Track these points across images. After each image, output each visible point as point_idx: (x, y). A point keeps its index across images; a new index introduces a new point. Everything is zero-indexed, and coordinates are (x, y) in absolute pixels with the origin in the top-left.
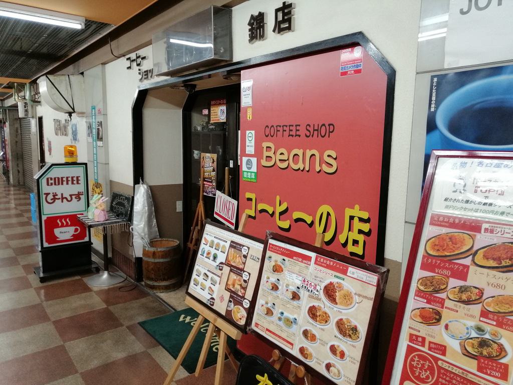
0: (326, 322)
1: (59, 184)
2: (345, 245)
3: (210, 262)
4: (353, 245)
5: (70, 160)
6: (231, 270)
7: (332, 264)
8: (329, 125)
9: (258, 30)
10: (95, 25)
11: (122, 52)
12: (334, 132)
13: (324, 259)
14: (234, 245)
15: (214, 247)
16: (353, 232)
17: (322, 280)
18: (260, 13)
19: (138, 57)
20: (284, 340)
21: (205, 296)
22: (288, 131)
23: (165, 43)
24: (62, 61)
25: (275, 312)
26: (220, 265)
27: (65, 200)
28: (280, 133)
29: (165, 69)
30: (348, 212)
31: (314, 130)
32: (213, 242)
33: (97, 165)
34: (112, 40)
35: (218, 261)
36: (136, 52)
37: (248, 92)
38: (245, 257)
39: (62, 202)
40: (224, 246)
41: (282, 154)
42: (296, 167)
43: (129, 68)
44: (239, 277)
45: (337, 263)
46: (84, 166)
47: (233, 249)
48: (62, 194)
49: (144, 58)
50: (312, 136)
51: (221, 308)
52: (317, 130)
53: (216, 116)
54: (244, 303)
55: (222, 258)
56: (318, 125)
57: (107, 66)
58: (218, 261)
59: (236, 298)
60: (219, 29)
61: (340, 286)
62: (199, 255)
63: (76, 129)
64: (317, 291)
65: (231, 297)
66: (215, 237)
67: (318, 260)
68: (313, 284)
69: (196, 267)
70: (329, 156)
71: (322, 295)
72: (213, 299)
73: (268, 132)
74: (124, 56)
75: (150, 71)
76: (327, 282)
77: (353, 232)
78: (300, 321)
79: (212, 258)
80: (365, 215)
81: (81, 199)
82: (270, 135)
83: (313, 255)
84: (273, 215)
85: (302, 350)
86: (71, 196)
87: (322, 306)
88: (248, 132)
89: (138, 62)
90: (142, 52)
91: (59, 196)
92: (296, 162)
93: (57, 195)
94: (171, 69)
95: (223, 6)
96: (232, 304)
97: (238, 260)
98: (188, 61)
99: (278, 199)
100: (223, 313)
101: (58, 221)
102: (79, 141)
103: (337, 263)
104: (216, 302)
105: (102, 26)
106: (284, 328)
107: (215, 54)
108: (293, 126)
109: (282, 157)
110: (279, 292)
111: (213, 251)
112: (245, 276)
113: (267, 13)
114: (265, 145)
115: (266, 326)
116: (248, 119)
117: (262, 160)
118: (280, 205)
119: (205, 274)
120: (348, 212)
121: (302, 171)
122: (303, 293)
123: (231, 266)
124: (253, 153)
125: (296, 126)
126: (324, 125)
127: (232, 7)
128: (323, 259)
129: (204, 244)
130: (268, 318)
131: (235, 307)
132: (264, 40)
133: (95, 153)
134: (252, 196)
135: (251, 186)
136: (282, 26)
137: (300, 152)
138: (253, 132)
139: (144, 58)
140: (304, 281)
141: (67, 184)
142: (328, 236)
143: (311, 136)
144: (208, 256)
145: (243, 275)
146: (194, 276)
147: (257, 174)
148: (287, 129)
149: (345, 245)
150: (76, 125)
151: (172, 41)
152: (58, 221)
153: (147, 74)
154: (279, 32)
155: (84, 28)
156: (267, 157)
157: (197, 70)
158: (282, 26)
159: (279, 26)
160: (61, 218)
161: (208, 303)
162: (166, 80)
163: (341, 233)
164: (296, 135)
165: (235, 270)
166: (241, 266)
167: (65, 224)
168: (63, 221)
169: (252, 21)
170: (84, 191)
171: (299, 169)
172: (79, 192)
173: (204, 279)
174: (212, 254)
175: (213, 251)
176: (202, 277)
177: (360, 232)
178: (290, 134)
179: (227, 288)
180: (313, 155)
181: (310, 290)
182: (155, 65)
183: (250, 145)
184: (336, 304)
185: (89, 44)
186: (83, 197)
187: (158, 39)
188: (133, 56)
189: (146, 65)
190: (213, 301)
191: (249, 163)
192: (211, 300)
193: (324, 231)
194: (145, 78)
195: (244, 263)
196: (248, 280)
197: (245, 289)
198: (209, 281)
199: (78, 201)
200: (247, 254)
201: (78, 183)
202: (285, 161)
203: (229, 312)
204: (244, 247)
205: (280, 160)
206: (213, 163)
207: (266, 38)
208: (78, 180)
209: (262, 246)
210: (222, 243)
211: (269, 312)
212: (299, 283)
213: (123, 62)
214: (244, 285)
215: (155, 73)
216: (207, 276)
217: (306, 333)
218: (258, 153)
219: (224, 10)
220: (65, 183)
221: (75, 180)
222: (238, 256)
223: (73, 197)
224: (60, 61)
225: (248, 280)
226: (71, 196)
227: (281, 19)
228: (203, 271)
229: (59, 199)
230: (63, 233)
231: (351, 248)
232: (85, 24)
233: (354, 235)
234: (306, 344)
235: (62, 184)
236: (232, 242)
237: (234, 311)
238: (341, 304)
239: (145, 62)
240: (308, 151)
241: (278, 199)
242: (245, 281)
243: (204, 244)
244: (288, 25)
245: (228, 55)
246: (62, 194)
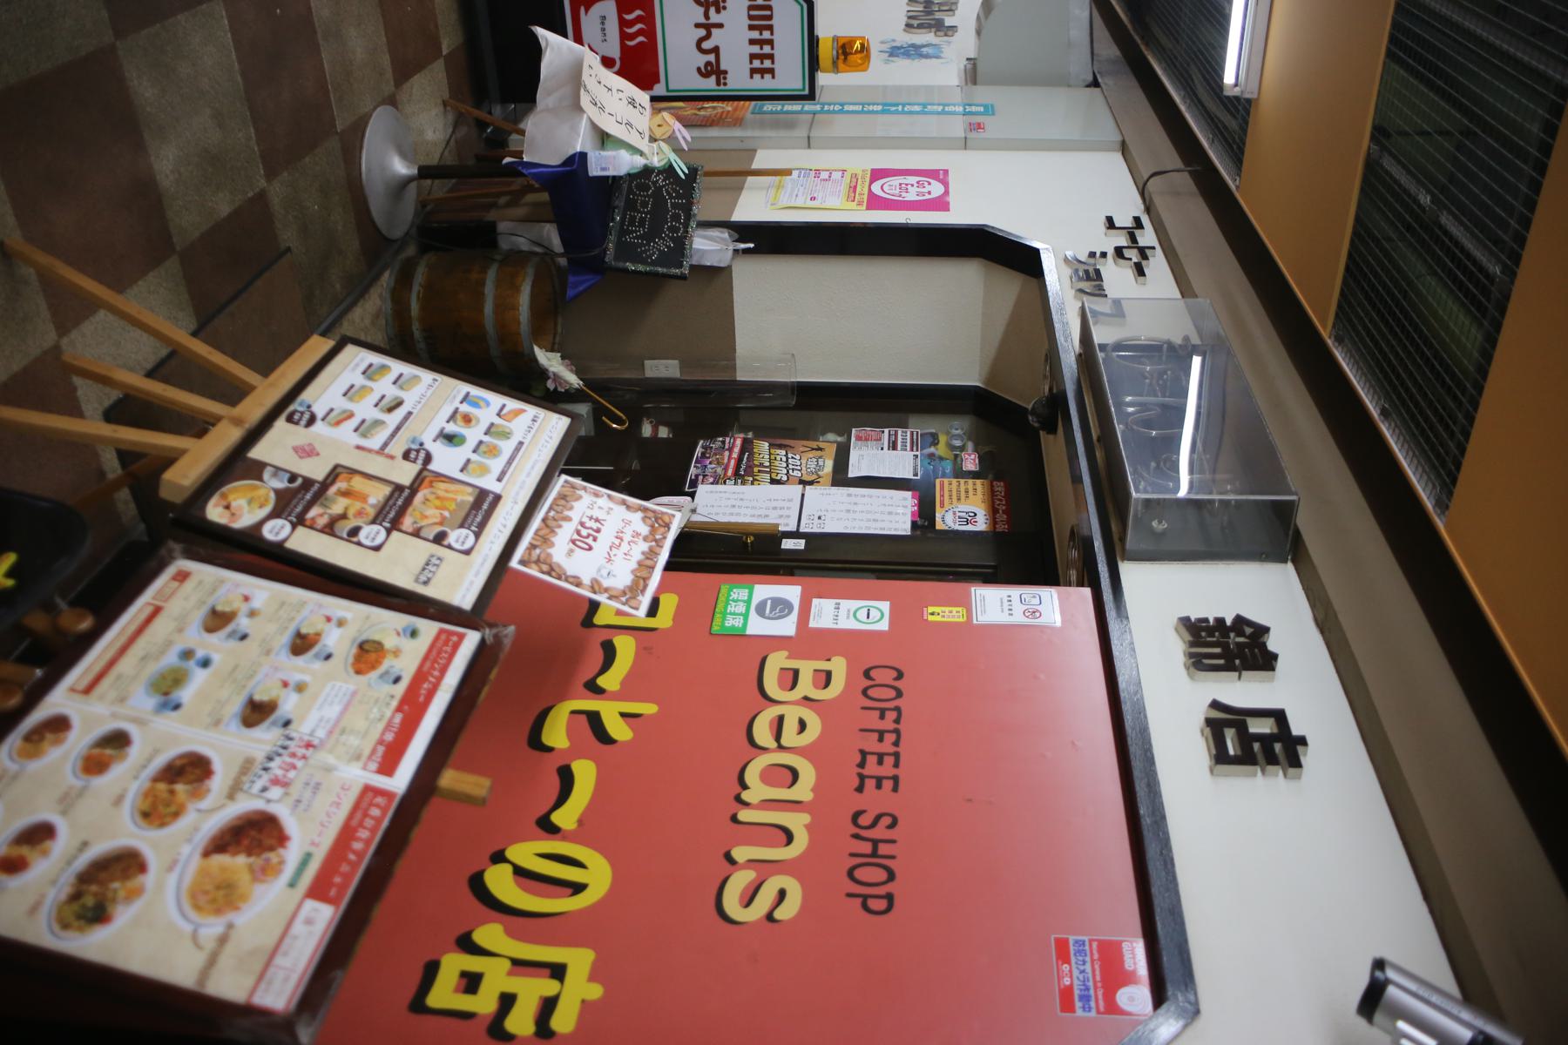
0: (146, 815)
1: (751, 18)
2: (467, 945)
3: (440, 422)
4: (464, 974)
5: (826, 51)
6: (398, 488)
7: (357, 846)
8: (889, 897)
9: (1217, 650)
10: (1237, 128)
11: (1159, 202)
12: (863, 913)
13: (378, 821)
14: (483, 505)
15: (486, 439)
16: (510, 973)
17: (302, 806)
18: (1275, 657)
19: (1143, 252)
20: (112, 663)
21: (324, 395)
23: (1186, 339)
24: (1129, 26)
25: (215, 639)
26: (422, 455)
27: (702, 32)
28: (873, 720)
29: (1100, 335)
30: (579, 960)
31: (875, 843)
32: (506, 435)
33: (807, 112)
34: (1193, 174)
35: (439, 451)
36: (1159, 249)
37: (1018, 609)
38: (439, 539)
39: (698, 26)
40: (484, 470)
41: (802, 726)
42: (752, 775)
43: (1110, 223)
44: (372, 512)
45: (354, 865)
46: (806, 92)
47: (471, 499)
48: (720, 26)
49: (1140, 271)
50: (856, 836)
51: (276, 447)
52: (874, 854)
53: (955, 497)
54: (278, 522)
55: (446, 460)
56: (893, 857)
57: (1118, 157)
58: (439, 451)
60: (1226, 518)
61: (265, 873)
62: (465, 388)
63: (927, 56)
64: (264, 789)
65: (308, 483)
66: (521, 443)
67: (379, 800)
68: (292, 774)
69: (427, 376)
70: (782, 894)
71: (245, 805)
72: (312, 420)
74: (1148, 210)
75: (1101, 288)
76: (290, 824)
77: (510, 973)
78: (168, 723)
79: (451, 428)
80: (563, 1021)
81: (707, 80)
82: (870, 683)
83: (400, 781)
84: (594, 689)
85: (59, 725)
86: (716, 50)
87: (205, 804)
88: (885, 606)
89: (1127, 253)
90: (1158, 265)
91: (715, 18)
92: (768, 776)
93: (718, 11)
94: (1100, 355)
95: (1297, 534)
96: (281, 484)
97: (433, 514)
98: (1127, 406)
99: (648, 709)
100: (257, 453)
101: (638, 12)
102: (887, 62)
103: (354, 865)
104: (300, 429)
105: (1236, 151)
106: (153, 668)
107: (1147, 502)
108: (896, 765)
109: (790, 727)
112: (372, 533)
113: (1272, 680)
114: (838, 666)
115: (174, 607)
116: (931, 609)
117: (784, 654)
118: (623, 715)
119: (399, 404)
120: (579, 960)
121: (738, 799)
122: (265, 737)
123: (414, 488)
124: (812, 624)
125: (895, 779)
126: (891, 876)
127: (1293, 561)
128: (380, 817)
129: (504, 406)
130: (198, 616)
131: (272, 495)
132: (1187, 669)
133: (846, 108)
135: (698, 614)
136: (1230, 735)
137: (803, 791)
138: (884, 626)
139: (1140, 271)
140: (309, 745)
141: (752, 42)
142: (500, 881)
143: (857, 831)
144: (458, 417)
145: (376, 527)
148: (886, 746)
149: (467, 945)
150: (938, 57)
151: (1197, 361)
152: (638, 12)
153: (1089, 277)
154: (1209, 722)
155: (1227, 93)
157: (1098, 440)
158: (1230, 735)
159: (1229, 724)
160: (649, 19)
161: (301, 405)
162: (1068, 336)
163: (510, 933)
164: (862, 778)
165: (400, 502)
166: (408, 522)
167: (631, 30)
168: (639, 26)
169: (1248, 631)
170: (726, 88)
171: (745, 787)
172: (725, 72)
173: (383, 397)
175: (473, 435)
176: (392, 392)
177: (507, 1001)
178: (867, 781)
179: (339, 470)
180: (789, 837)
181: (272, 765)
182: (1117, 303)
183: (843, 612)
184: (207, 854)
185: (1183, 108)
186: (710, 84)
187: (1197, 318)
188: (1147, 237)
189: (1117, 278)
190: (303, 422)
191: (782, 607)
192: (307, 416)
193: (520, 872)
194: (1076, 271)
195: (416, 534)
196: (359, 544)
197: (329, 529)
199: (699, 69)
200: (449, 547)
201: (753, 71)
202: (778, 737)
203: (256, 470)
204: (472, 538)
205: (781, 719)
207: (1191, 676)
208: (763, 72)
210: (497, 465)
213: (1128, 207)
214: (344, 528)
215: (1093, 304)
216: (390, 410)
217: (118, 740)
218: (810, 642)
219: (1287, 535)
220: (755, 35)
221: (762, 63)
222: (446, 514)
223: (712, 58)
224: (1131, 21)
225: (359, 544)
226: (716, 50)
227: (1252, 730)
228: (411, 398)
229: (707, 16)
230: (603, 23)
231: (454, 964)
232: (1237, 98)
233: (497, 977)
234: (78, 741)
235: (751, 28)
236: (498, 498)
237: (256, 488)
238: (203, 873)
239: (1128, 273)
240: (805, 818)
241: (648, 709)
242: (354, 532)
243: (504, 406)
244: (1231, 752)
245: (1143, 546)
246: (720, 26)
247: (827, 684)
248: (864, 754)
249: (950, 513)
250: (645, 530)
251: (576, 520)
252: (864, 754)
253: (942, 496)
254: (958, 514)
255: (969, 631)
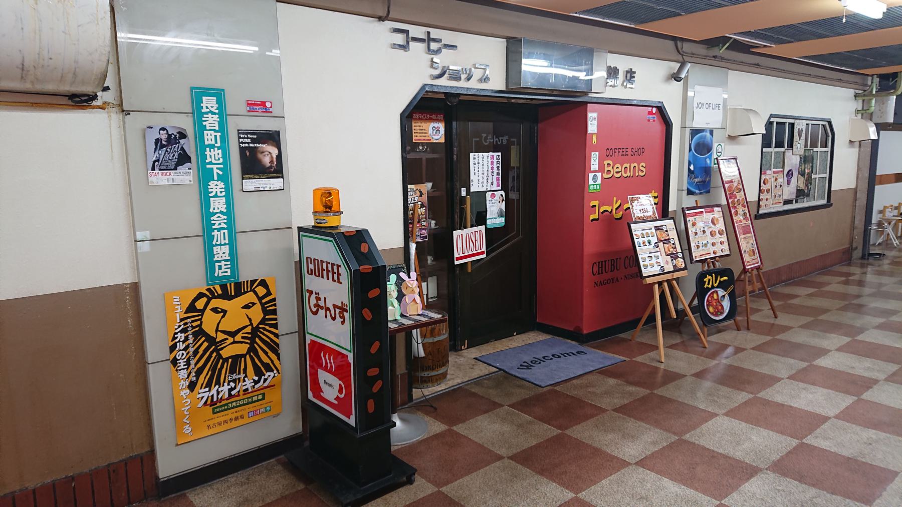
3: (648, 247)
6: (663, 243)
14: (658, 228)
15: (645, 237)
21: (656, 270)
22: (621, 152)
32: (642, 234)
35: (653, 243)
37: (593, 122)
38: (667, 231)
40: (652, 233)
41: (617, 168)
44: (669, 244)
53: (426, 135)
54: (679, 256)
55: (654, 240)
58: (653, 243)
59: (674, 256)
62: (638, 248)
69: (640, 257)
70: (642, 166)
72: (663, 267)
73: (608, 153)
79: (647, 244)
83: (703, 210)
92: (626, 172)
97: (664, 235)
99: (615, 199)
109: (618, 170)
110: (698, 235)
111: (646, 239)
114: (606, 162)
117: (604, 174)
123: (661, 241)
134: (596, 203)
137: (627, 165)
146: (642, 263)
147: (601, 185)
156: (607, 171)
166: (667, 238)
174: (646, 241)
175: (646, 239)
176: (647, 260)
180: (635, 166)
191: (595, 177)
195: (668, 235)
197: (675, 248)
198: (654, 259)
202: (619, 172)
203: (675, 266)
205: (616, 172)
206: (421, 196)
209: (672, 220)
210: (649, 231)
211: (698, 247)
212: (703, 225)
214: (673, 246)
216: (651, 257)
218: (601, 169)
230: (327, 383)
236: (655, 227)
241: (615, 199)
242: (673, 244)
247: (610, 164)
248: (622, 155)
249: (434, 137)
250: (636, 202)
251: (643, 214)
252: (622, 155)
253: (424, 140)
254: (434, 134)
255: (598, 134)
